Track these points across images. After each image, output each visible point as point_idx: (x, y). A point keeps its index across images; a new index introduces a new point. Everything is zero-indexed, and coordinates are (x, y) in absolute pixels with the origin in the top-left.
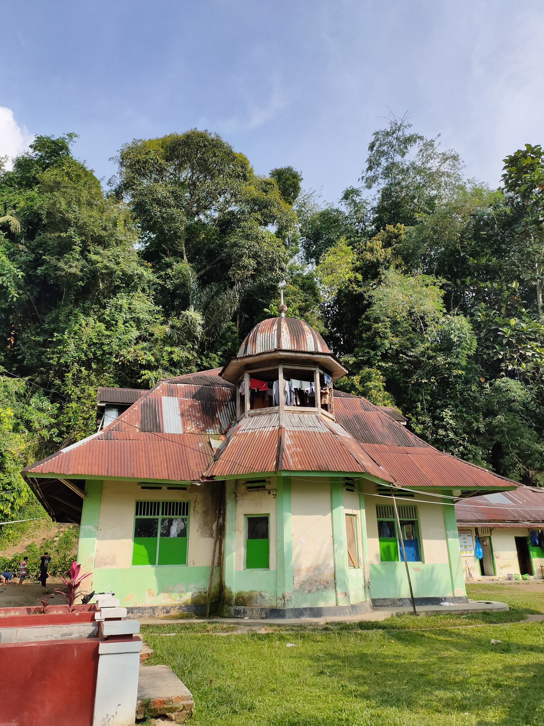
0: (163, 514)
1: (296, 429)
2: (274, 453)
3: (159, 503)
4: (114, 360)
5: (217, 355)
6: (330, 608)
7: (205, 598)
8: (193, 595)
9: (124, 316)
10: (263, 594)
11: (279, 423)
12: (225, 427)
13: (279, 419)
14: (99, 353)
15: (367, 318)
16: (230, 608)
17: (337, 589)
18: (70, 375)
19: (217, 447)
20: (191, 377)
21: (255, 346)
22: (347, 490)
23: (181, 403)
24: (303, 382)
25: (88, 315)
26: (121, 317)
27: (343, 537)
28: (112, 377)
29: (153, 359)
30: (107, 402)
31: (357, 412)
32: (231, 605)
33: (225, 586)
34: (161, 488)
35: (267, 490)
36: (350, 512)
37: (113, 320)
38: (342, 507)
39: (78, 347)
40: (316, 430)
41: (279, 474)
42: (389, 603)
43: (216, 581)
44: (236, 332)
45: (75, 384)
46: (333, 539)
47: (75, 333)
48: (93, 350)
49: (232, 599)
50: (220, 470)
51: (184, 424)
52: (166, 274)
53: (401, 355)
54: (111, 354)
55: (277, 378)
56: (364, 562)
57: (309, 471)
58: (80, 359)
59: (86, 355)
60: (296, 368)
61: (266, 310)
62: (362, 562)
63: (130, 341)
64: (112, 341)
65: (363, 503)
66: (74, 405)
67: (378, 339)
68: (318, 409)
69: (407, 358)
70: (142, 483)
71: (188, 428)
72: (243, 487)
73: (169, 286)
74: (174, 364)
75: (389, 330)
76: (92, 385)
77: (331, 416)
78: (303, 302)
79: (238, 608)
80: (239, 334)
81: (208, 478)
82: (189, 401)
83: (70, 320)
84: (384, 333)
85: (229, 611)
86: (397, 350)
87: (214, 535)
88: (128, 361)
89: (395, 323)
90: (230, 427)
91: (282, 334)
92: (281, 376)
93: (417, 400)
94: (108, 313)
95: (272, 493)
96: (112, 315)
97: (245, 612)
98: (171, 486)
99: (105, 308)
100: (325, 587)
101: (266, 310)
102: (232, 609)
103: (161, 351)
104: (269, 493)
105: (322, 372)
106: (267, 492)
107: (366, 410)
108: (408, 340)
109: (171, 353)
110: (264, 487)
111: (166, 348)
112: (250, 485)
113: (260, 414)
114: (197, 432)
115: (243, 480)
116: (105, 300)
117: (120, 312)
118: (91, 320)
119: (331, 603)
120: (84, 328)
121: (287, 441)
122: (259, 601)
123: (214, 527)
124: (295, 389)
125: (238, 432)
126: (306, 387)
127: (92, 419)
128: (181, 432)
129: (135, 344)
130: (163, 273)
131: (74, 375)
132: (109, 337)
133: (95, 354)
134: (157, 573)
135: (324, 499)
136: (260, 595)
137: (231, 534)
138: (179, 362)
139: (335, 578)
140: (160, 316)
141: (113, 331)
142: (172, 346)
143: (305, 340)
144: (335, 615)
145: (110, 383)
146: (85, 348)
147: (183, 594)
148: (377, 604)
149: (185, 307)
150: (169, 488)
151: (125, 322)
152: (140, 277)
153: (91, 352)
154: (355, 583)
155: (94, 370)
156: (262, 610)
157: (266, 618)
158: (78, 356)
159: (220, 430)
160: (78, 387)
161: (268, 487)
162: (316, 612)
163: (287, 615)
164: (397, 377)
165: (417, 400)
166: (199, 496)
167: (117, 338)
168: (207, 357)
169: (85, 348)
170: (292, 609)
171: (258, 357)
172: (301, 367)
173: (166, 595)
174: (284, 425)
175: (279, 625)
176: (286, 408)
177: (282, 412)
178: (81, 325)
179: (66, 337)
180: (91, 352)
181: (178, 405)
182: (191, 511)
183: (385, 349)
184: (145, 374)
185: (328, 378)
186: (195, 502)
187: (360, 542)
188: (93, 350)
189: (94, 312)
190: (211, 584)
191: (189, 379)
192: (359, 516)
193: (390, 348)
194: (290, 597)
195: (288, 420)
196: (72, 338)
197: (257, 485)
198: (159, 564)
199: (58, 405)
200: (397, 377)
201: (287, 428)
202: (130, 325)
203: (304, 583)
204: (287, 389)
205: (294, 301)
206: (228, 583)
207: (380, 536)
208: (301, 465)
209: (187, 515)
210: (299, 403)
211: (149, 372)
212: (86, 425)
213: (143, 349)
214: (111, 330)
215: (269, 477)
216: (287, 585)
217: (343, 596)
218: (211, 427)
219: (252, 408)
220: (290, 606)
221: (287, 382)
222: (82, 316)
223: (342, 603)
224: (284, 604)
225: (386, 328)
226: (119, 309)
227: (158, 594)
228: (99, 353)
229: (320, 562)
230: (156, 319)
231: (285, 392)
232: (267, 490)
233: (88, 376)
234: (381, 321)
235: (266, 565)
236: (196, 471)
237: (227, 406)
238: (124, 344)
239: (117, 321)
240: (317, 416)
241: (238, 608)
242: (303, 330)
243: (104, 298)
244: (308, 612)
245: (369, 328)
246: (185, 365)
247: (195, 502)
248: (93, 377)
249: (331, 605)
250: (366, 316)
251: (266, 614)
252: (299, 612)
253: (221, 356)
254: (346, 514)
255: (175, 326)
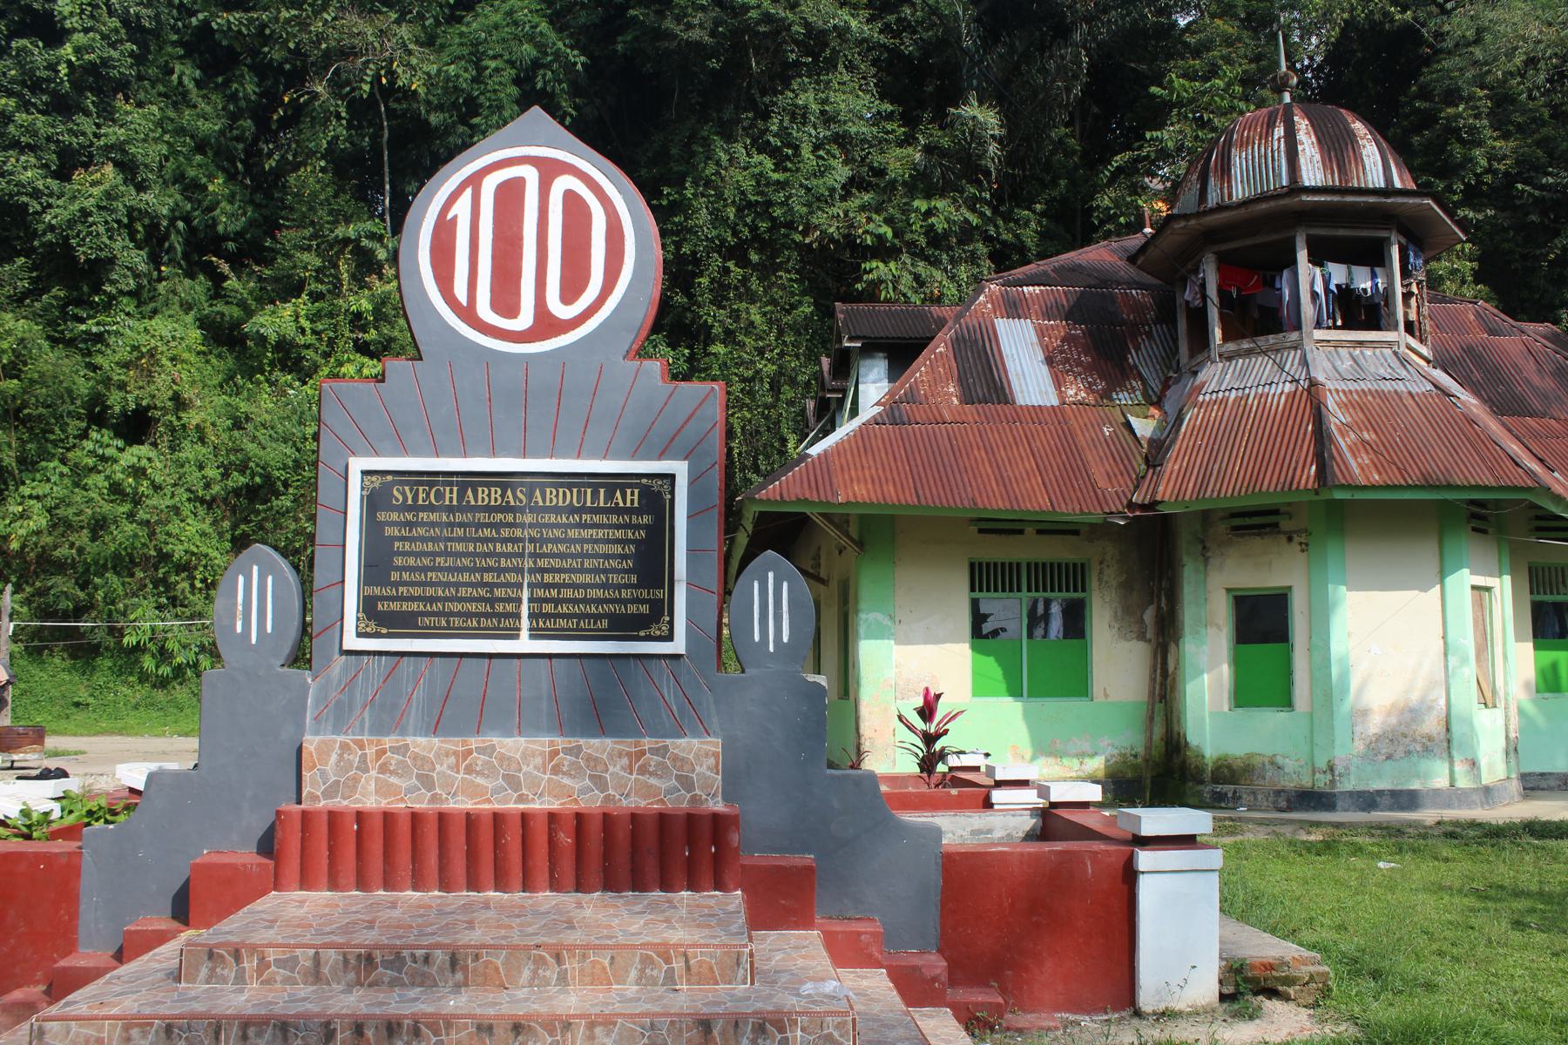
0: (1029, 590)
1: (1352, 386)
2: (1307, 447)
3: (1018, 565)
4: (798, 238)
5: (1034, 212)
6: (1436, 791)
7: (1135, 767)
8: (1107, 761)
9: (813, 132)
10: (1279, 760)
11: (1308, 372)
12: (1155, 385)
13: (1304, 362)
14: (763, 225)
15: (1425, 94)
16: (1200, 787)
17: (1454, 753)
18: (704, 281)
19: (1148, 434)
20: (1048, 269)
21: (1229, 182)
22: (1474, 529)
23: (1041, 332)
24: (1354, 268)
25: (729, 138)
26: (806, 137)
27: (1466, 639)
28: (795, 281)
29: (890, 234)
30: (864, 337)
31: (1470, 338)
32: (1202, 782)
33: (1187, 743)
34: (1021, 532)
35: (1285, 533)
36: (1480, 581)
37: (789, 146)
38: (1466, 571)
39: (718, 219)
40: (1400, 387)
41: (1325, 495)
42: (1552, 783)
43: (1159, 731)
44: (1074, 152)
45: (718, 302)
46: (1445, 643)
47: (708, 184)
48: (748, 220)
49: (1203, 771)
50: (1171, 487)
51: (1058, 384)
52: (899, 20)
53: (1520, 186)
54: (790, 225)
55: (1293, 262)
56: (1506, 694)
57: (1401, 487)
58: (723, 241)
59: (735, 234)
60: (1341, 232)
61: (1154, 89)
62: (1501, 693)
63: (832, 190)
64: (790, 196)
65: (1506, 560)
66: (719, 348)
67: (1457, 150)
68: (1398, 336)
69: (1537, 193)
70: (980, 520)
71: (1071, 392)
72: (1222, 528)
73: (908, 46)
74: (936, 240)
75: (1485, 122)
76: (753, 302)
77: (1424, 351)
78: (1251, 61)
79: (1219, 788)
80: (1081, 158)
81: (1143, 507)
82: (1059, 327)
83: (693, 154)
84: (1472, 130)
85: (1200, 793)
86: (1506, 174)
87: (1149, 636)
88: (832, 240)
89: (1503, 100)
90: (1166, 385)
91: (1300, 148)
92: (1302, 256)
93: (1557, 302)
94: (774, 128)
95: (1296, 539)
96: (783, 133)
97: (1237, 798)
98: (1041, 526)
99: (766, 116)
100: (1426, 749)
101: (1154, 89)
102: (1207, 790)
103: (906, 210)
104: (1290, 539)
105: (1403, 241)
106: (1283, 538)
107: (1492, 332)
108: (1538, 144)
109: (929, 213)
110: (1276, 525)
111: (916, 203)
112: (1238, 522)
113: (1249, 353)
114: (1091, 400)
115: (1223, 510)
116: (767, 99)
117: (804, 124)
118: (739, 149)
119: (1441, 782)
120: (726, 169)
121: (1336, 417)
122: (1269, 774)
123: (1149, 616)
124: (1338, 286)
125: (1201, 398)
126: (1363, 282)
127: (761, 380)
128: (1055, 402)
129: (843, 199)
130: (892, 18)
131: (712, 281)
132: (781, 185)
133: (753, 228)
134: (1027, 715)
135: (1425, 552)
136: (1272, 763)
137: (1198, 632)
138: (946, 234)
139: (1448, 730)
140: (895, 126)
141: (789, 170)
142: (928, 197)
143: (1359, 159)
144: (1449, 806)
145: (793, 294)
146: (732, 216)
147: (1087, 760)
148: (1534, 785)
149: (957, 98)
150: (1039, 532)
151: (816, 148)
152: (842, 32)
153: (746, 225)
154: (1489, 736)
155: (755, 267)
156: (1278, 793)
157: (1289, 809)
158: (718, 237)
159: (1145, 394)
160: (724, 308)
161: (1285, 524)
162: (1407, 799)
163: (1339, 804)
164: (1506, 246)
165: (1557, 302)
166: (1110, 550)
167: (801, 185)
168: (1008, 218)
169: (732, 216)
170: (1351, 793)
171: (1242, 210)
172: (1351, 229)
173: (1051, 760)
174: (1321, 378)
175: (1337, 825)
176: (1319, 334)
177: (1308, 346)
178: (718, 163)
179: (689, 193)
180: (746, 225)
181: (1035, 339)
182: (1094, 583)
183: (1476, 175)
184: (871, 270)
185: (1416, 256)
186: (1101, 563)
187: (1498, 650)
188: (748, 220)
189: (744, 129)
190: (1151, 739)
191: (1045, 272)
192: (1497, 591)
193: (1489, 170)
194: (1347, 768)
195: (1327, 365)
196: (703, 195)
197: (1258, 522)
198: (1032, 694)
199: (687, 351)
200: (1506, 246)
201: (1329, 385)
202: (828, 152)
203: (1379, 738)
204: (1319, 288)
205: (1228, 60)
206: (1193, 738)
207: (1535, 636)
208: (1380, 473)
209: (1084, 590)
210: (1339, 323)
211: (881, 265)
212: (751, 393)
213: (863, 208)
214: (786, 170)
215: (1289, 504)
216: (1337, 743)
217: (1466, 767)
218: (1123, 388)
219: (1225, 339)
220: (1348, 785)
221: (1318, 270)
222: (718, 142)
223: (1463, 782)
224: (1333, 782)
225: (1476, 117)
226: (799, 115)
227: (1033, 759)
228: (763, 225)
229: (1415, 697)
230: (887, 133)
231: (1315, 295)
232: (1285, 533)
233: (744, 281)
234: (1461, 98)
235: (1286, 701)
236: (1109, 492)
237: (1149, 335)
238: (818, 199)
239: (797, 148)
240: (1395, 353)
241: (1219, 788)
242: (1352, 137)
243: (763, 94)
244: (1386, 801)
245: (1428, 119)
246: (960, 242)
247: (1101, 563)
248: (754, 284)
249: (1438, 786)
250: (1421, 88)
251: (1288, 801)
252: (1368, 800)
253: (1043, 214)
254: (1474, 588)
255: (936, 147)
